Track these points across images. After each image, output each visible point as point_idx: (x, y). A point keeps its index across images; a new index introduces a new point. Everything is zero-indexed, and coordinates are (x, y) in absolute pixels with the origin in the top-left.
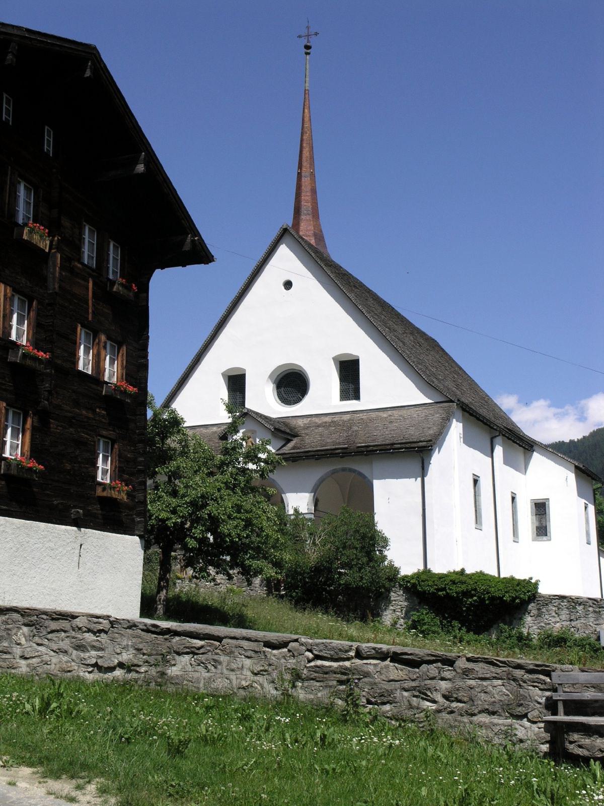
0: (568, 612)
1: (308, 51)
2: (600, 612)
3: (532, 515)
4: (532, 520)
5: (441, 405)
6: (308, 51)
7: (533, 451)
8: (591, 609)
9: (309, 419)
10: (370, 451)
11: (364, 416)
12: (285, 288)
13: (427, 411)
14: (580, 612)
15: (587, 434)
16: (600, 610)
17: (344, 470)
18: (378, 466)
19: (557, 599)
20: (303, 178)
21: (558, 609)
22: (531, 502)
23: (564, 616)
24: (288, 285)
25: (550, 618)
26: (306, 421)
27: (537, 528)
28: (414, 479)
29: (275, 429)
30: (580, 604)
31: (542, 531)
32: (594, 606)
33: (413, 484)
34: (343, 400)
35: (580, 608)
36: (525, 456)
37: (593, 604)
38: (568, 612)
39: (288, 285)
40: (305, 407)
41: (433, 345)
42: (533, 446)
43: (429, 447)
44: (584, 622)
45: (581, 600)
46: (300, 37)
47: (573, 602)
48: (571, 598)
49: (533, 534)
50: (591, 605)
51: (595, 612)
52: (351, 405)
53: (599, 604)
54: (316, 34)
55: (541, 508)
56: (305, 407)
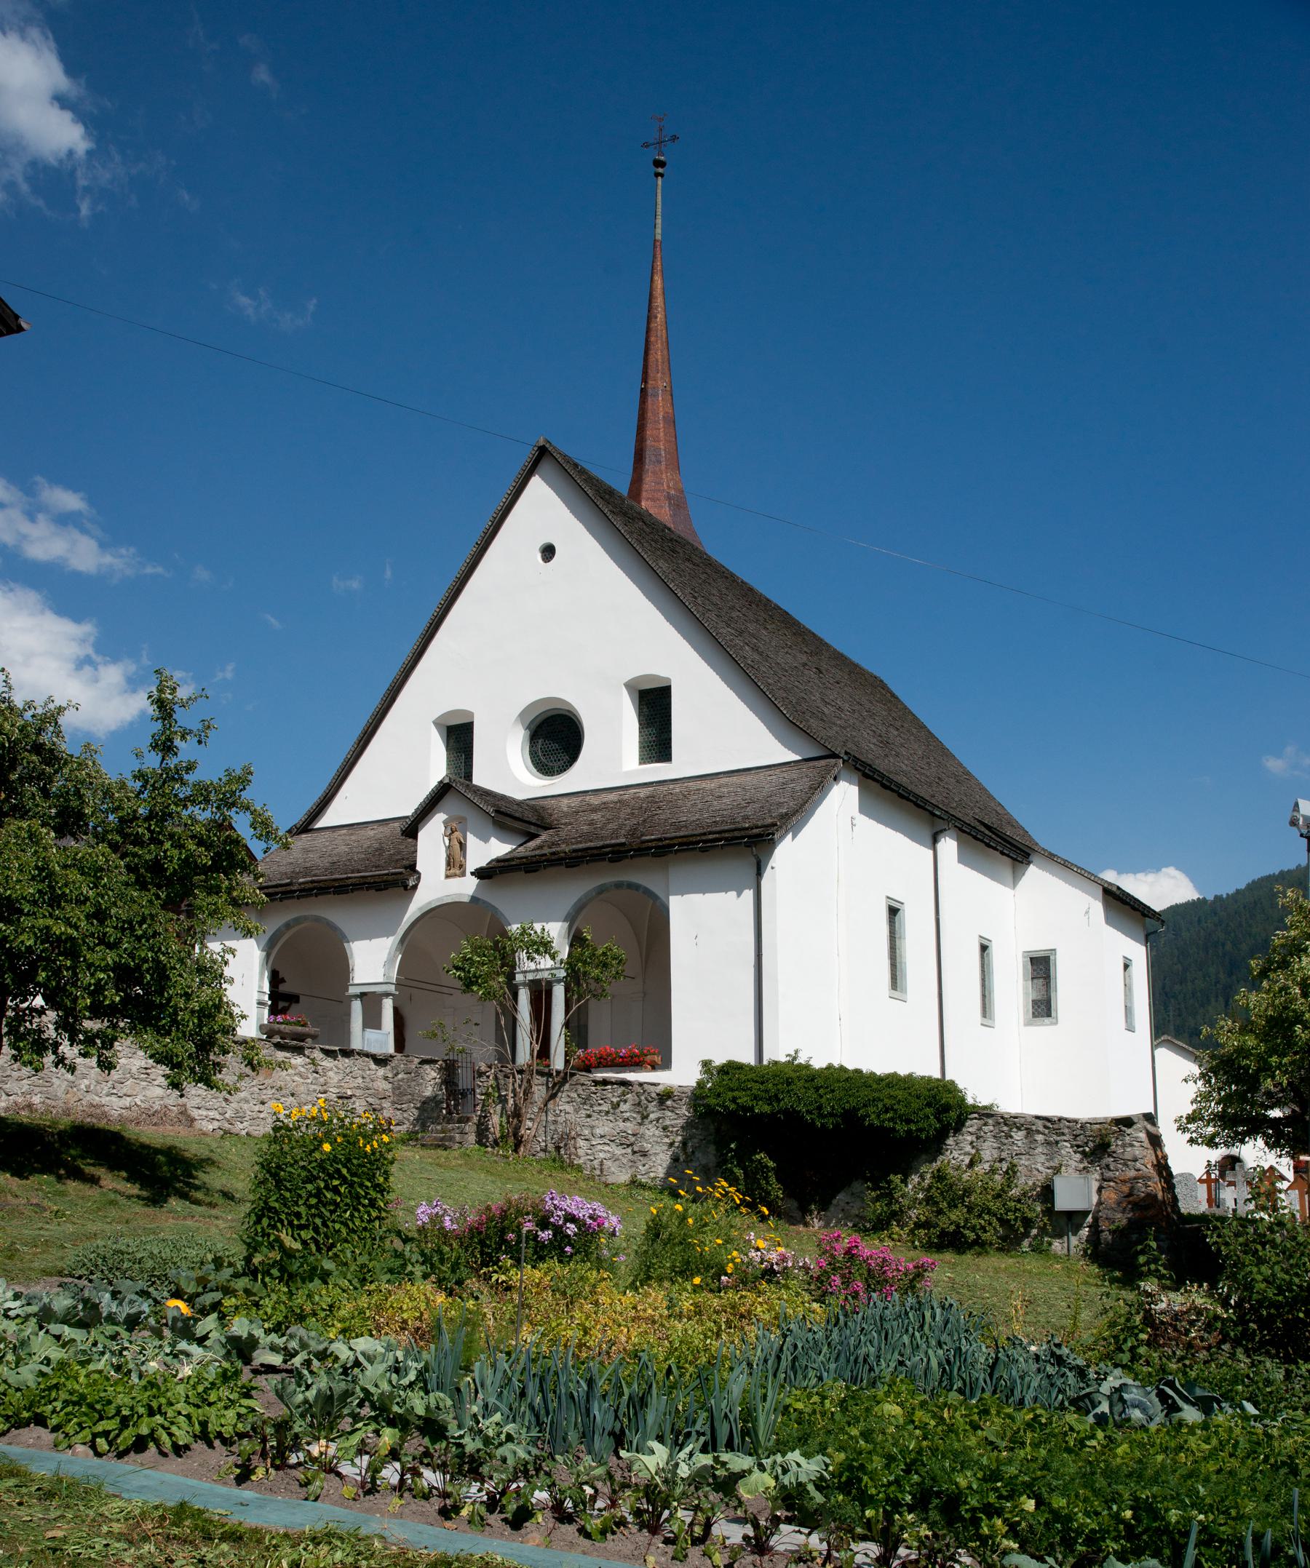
0: (995, 1145)
1: (660, 170)
2: (1057, 1143)
3: (1025, 980)
4: (1025, 988)
5: (816, 763)
6: (660, 170)
7: (1029, 863)
8: (1040, 1138)
9: (580, 799)
10: (664, 847)
11: (677, 789)
12: (543, 559)
13: (794, 774)
14: (1020, 1143)
15: (1242, 886)
16: (1058, 1138)
17: (619, 885)
18: (679, 871)
19: (976, 1118)
20: (649, 399)
21: (978, 1138)
22: (1024, 957)
23: (988, 1152)
24: (548, 552)
25: (962, 1157)
26: (575, 802)
27: (1035, 1003)
28: (734, 893)
29: (497, 811)
30: (1019, 1129)
31: (1043, 1008)
32: (1047, 1131)
33: (736, 904)
34: (645, 763)
35: (1019, 1136)
36: (1014, 872)
37: (1045, 1127)
38: (995, 1145)
39: (548, 552)
40: (576, 779)
41: (876, 685)
42: (1029, 855)
43: (768, 835)
44: (1026, 1163)
45: (1022, 1121)
46: (646, 145)
47: (1006, 1124)
48: (1002, 1118)
49: (1026, 1013)
50: (1041, 1129)
51: (1048, 1143)
52: (658, 771)
53: (1056, 1126)
54: (674, 138)
55: (1041, 967)
56: (576, 779)
